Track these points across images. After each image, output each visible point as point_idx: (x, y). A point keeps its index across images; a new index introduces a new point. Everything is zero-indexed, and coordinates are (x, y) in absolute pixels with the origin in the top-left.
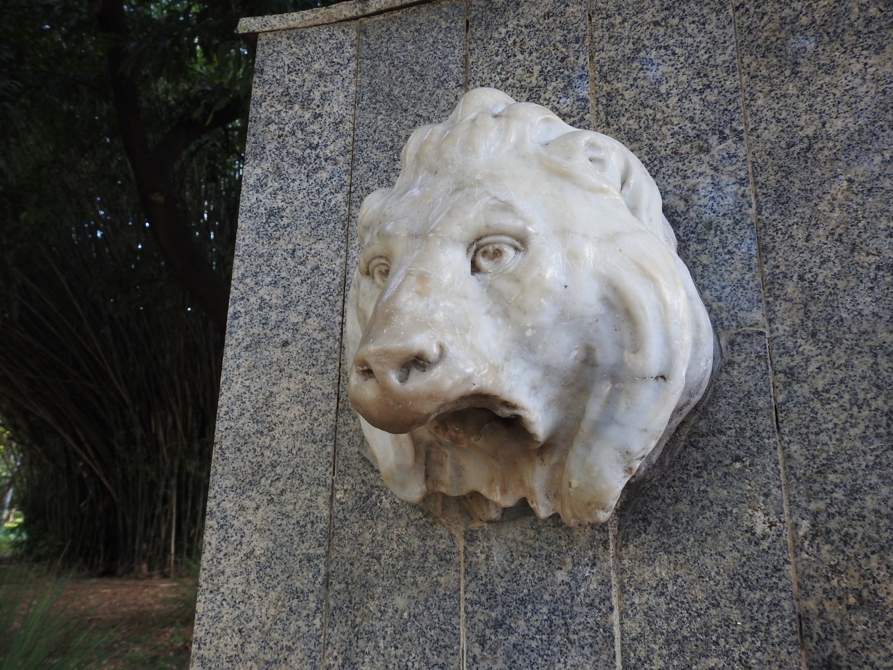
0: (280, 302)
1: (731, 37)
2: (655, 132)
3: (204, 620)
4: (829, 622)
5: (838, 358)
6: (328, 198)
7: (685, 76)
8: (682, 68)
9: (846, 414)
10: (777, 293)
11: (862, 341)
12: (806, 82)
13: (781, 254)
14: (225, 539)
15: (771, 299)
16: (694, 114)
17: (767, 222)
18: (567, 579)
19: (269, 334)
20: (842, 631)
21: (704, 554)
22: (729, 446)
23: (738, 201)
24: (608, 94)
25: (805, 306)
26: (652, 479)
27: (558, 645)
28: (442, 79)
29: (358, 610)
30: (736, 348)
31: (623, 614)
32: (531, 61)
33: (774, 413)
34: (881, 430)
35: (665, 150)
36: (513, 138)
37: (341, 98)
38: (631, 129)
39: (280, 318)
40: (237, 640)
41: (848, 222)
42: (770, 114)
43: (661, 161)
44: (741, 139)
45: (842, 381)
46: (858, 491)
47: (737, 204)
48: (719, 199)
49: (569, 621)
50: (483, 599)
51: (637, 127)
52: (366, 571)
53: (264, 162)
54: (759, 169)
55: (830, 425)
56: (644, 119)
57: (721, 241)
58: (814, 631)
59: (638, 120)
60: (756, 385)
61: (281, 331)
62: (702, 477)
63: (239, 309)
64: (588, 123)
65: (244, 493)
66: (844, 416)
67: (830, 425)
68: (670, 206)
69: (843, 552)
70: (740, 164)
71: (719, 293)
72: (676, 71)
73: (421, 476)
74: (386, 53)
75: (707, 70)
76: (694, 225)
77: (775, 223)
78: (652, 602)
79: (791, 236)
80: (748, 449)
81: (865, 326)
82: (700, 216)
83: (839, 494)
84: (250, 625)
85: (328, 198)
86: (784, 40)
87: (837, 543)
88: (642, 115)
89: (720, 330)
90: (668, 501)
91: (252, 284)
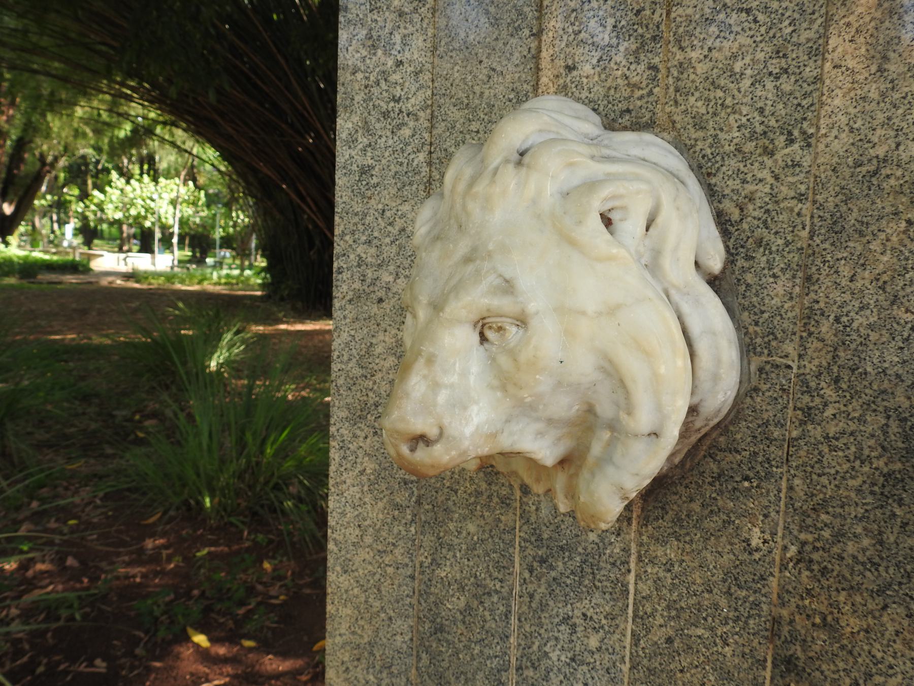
0: (374, 261)
1: (822, 6)
2: (722, 121)
3: (334, 514)
4: (796, 630)
5: (854, 410)
6: (411, 157)
7: (763, 53)
8: (761, 42)
9: (848, 465)
10: (812, 329)
11: (879, 399)
12: (890, 86)
13: (823, 289)
14: (344, 458)
15: (804, 334)
16: (766, 104)
17: (817, 250)
18: (597, 540)
19: (367, 290)
20: (804, 641)
21: (707, 549)
24: (681, 64)
25: (836, 349)
26: (673, 476)
27: (586, 586)
28: (516, 25)
29: (441, 527)
30: (764, 376)
31: (638, 577)
33: (786, 446)
34: (876, 489)
37: (420, 43)
38: (698, 113)
39: (375, 277)
40: (357, 532)
41: (895, 270)
42: (844, 120)
43: (723, 158)
44: (809, 145)
45: (852, 434)
46: (843, 535)
48: (774, 213)
49: (596, 572)
50: (533, 539)
51: (704, 112)
52: (447, 500)
53: (354, 115)
55: (833, 471)
56: (712, 103)
57: (768, 261)
58: (783, 634)
60: (775, 416)
61: (376, 289)
63: (342, 264)
64: (656, 99)
66: (846, 466)
67: (833, 471)
69: (819, 581)
70: (802, 175)
72: (754, 45)
75: (787, 48)
77: (824, 253)
78: (661, 574)
79: (837, 272)
80: (758, 472)
81: (886, 385)
83: (826, 534)
84: (366, 523)
85: (411, 157)
86: (878, 22)
87: (816, 572)
88: (712, 97)
89: (752, 354)
91: (351, 242)
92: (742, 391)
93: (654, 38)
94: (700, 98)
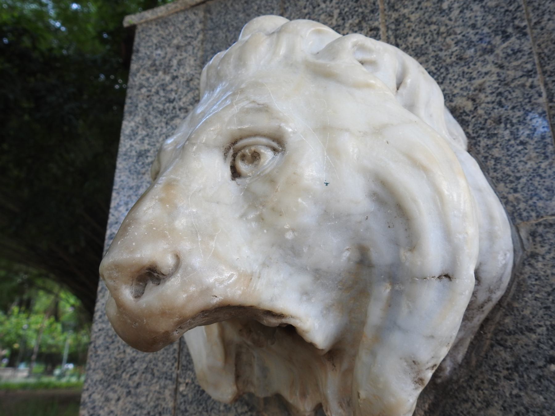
16: (476, 21)
22: (541, 345)
23: (526, 92)
30: (538, 239)
32: (332, 7)
35: (451, 58)
36: (282, 51)
37: (192, 62)
44: (525, 34)
47: (525, 96)
54: (546, 59)
57: (512, 133)
59: (424, 37)
62: (513, 380)
65: (109, 386)
68: (458, 107)
71: (514, 184)
73: (231, 378)
74: (224, 23)
76: (483, 122)
82: (488, 112)
89: (518, 221)
90: (478, 405)
92: (518, 260)
93: (372, 11)
94: (418, 36)
